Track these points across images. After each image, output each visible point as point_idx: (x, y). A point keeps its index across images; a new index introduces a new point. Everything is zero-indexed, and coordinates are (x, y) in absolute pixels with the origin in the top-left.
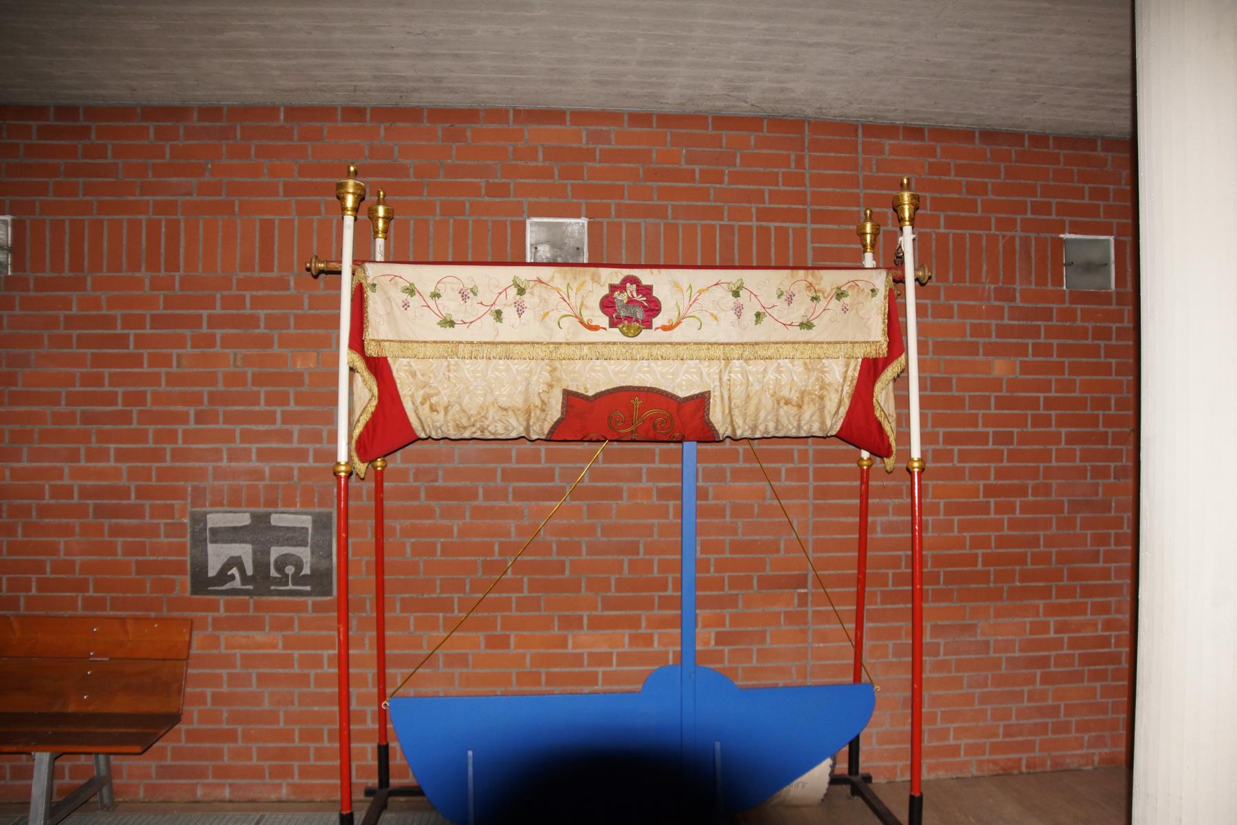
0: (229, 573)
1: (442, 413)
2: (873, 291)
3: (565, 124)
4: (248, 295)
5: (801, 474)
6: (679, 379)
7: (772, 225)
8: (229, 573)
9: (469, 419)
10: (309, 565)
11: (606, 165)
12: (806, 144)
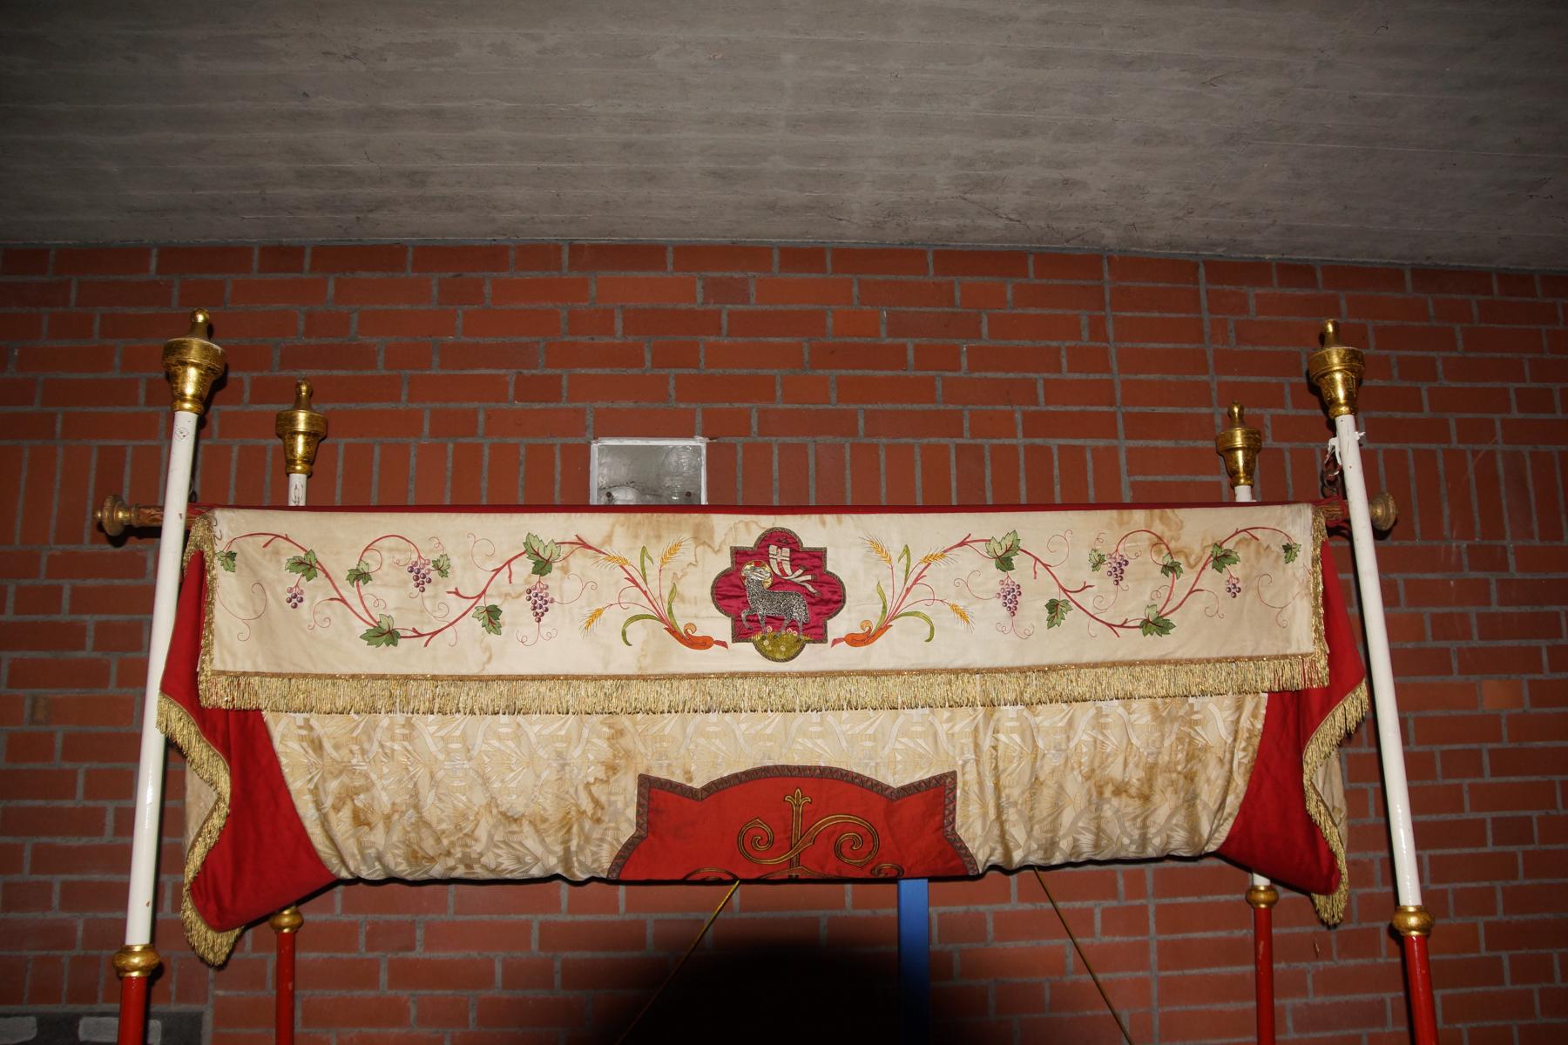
1: (381, 827)
2: (1287, 548)
3: (665, 269)
4: (67, 585)
5: (1132, 920)
6: (887, 751)
7: (1054, 443)
9: (438, 840)
11: (739, 340)
12: (1107, 297)
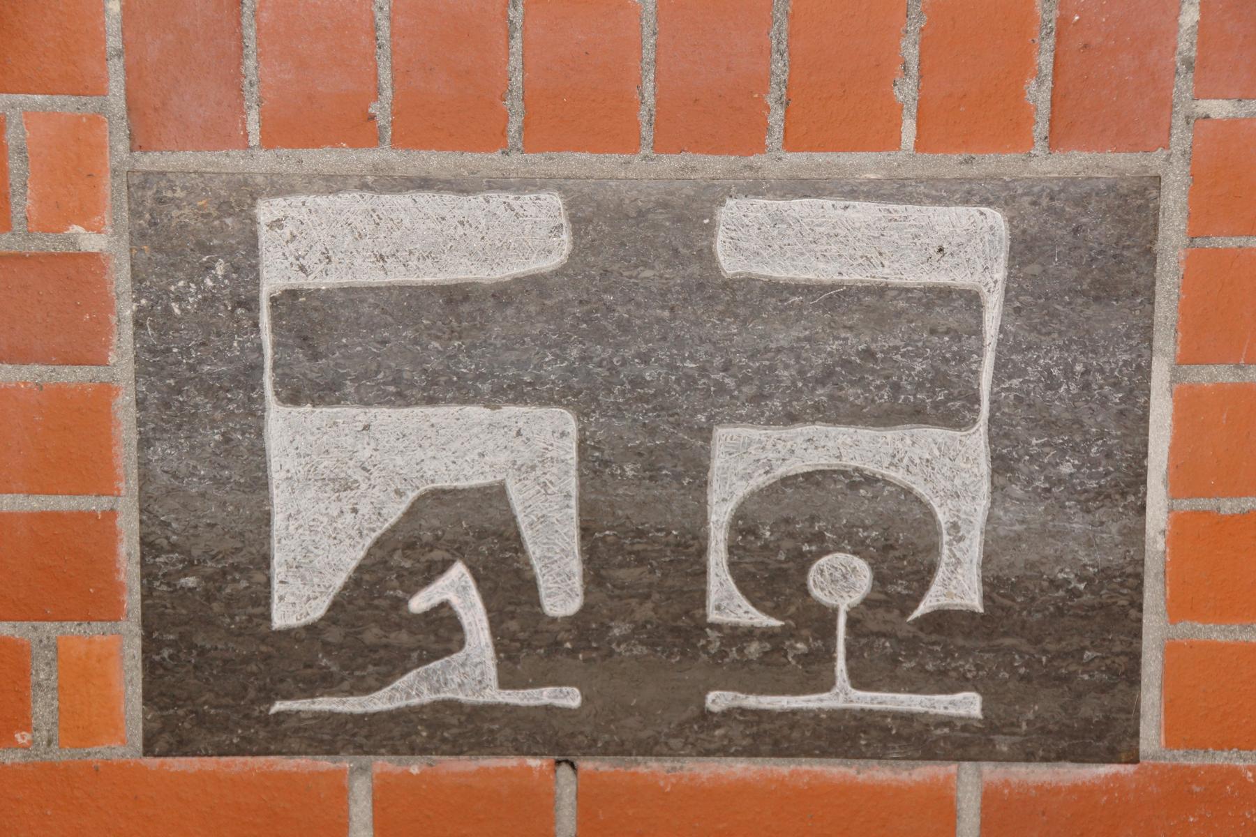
0: (419, 603)
8: (419, 603)
10: (973, 547)
